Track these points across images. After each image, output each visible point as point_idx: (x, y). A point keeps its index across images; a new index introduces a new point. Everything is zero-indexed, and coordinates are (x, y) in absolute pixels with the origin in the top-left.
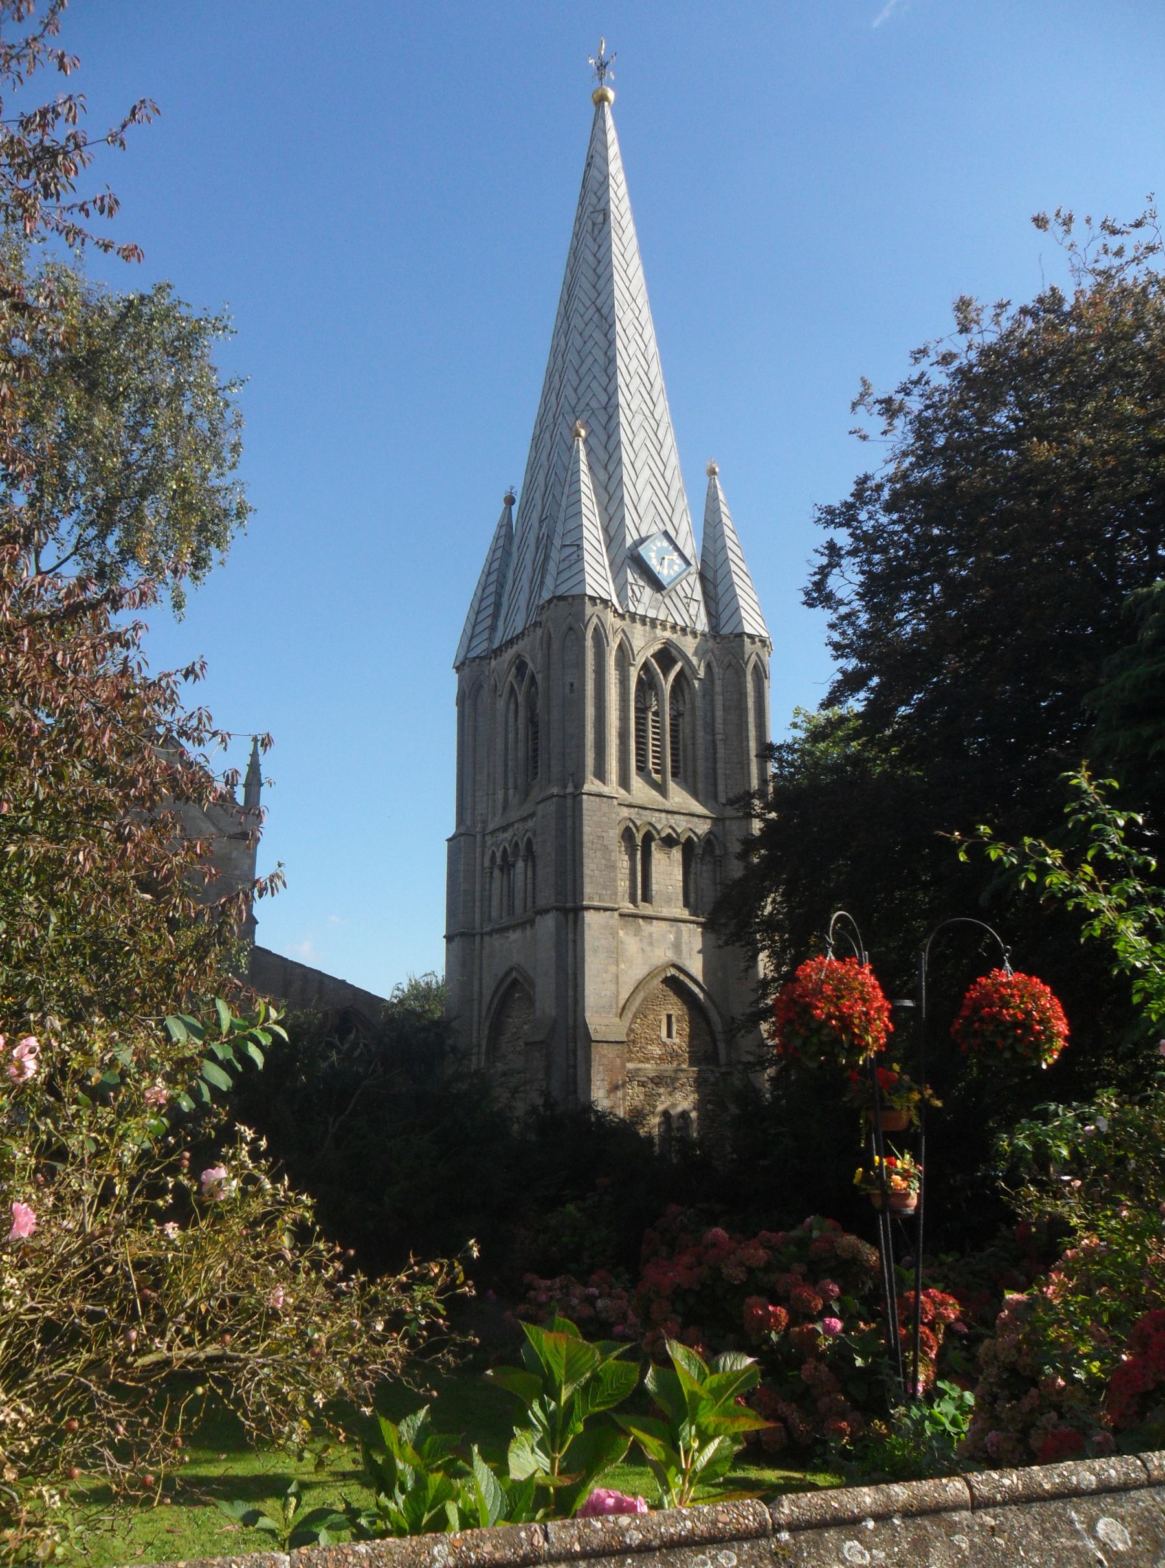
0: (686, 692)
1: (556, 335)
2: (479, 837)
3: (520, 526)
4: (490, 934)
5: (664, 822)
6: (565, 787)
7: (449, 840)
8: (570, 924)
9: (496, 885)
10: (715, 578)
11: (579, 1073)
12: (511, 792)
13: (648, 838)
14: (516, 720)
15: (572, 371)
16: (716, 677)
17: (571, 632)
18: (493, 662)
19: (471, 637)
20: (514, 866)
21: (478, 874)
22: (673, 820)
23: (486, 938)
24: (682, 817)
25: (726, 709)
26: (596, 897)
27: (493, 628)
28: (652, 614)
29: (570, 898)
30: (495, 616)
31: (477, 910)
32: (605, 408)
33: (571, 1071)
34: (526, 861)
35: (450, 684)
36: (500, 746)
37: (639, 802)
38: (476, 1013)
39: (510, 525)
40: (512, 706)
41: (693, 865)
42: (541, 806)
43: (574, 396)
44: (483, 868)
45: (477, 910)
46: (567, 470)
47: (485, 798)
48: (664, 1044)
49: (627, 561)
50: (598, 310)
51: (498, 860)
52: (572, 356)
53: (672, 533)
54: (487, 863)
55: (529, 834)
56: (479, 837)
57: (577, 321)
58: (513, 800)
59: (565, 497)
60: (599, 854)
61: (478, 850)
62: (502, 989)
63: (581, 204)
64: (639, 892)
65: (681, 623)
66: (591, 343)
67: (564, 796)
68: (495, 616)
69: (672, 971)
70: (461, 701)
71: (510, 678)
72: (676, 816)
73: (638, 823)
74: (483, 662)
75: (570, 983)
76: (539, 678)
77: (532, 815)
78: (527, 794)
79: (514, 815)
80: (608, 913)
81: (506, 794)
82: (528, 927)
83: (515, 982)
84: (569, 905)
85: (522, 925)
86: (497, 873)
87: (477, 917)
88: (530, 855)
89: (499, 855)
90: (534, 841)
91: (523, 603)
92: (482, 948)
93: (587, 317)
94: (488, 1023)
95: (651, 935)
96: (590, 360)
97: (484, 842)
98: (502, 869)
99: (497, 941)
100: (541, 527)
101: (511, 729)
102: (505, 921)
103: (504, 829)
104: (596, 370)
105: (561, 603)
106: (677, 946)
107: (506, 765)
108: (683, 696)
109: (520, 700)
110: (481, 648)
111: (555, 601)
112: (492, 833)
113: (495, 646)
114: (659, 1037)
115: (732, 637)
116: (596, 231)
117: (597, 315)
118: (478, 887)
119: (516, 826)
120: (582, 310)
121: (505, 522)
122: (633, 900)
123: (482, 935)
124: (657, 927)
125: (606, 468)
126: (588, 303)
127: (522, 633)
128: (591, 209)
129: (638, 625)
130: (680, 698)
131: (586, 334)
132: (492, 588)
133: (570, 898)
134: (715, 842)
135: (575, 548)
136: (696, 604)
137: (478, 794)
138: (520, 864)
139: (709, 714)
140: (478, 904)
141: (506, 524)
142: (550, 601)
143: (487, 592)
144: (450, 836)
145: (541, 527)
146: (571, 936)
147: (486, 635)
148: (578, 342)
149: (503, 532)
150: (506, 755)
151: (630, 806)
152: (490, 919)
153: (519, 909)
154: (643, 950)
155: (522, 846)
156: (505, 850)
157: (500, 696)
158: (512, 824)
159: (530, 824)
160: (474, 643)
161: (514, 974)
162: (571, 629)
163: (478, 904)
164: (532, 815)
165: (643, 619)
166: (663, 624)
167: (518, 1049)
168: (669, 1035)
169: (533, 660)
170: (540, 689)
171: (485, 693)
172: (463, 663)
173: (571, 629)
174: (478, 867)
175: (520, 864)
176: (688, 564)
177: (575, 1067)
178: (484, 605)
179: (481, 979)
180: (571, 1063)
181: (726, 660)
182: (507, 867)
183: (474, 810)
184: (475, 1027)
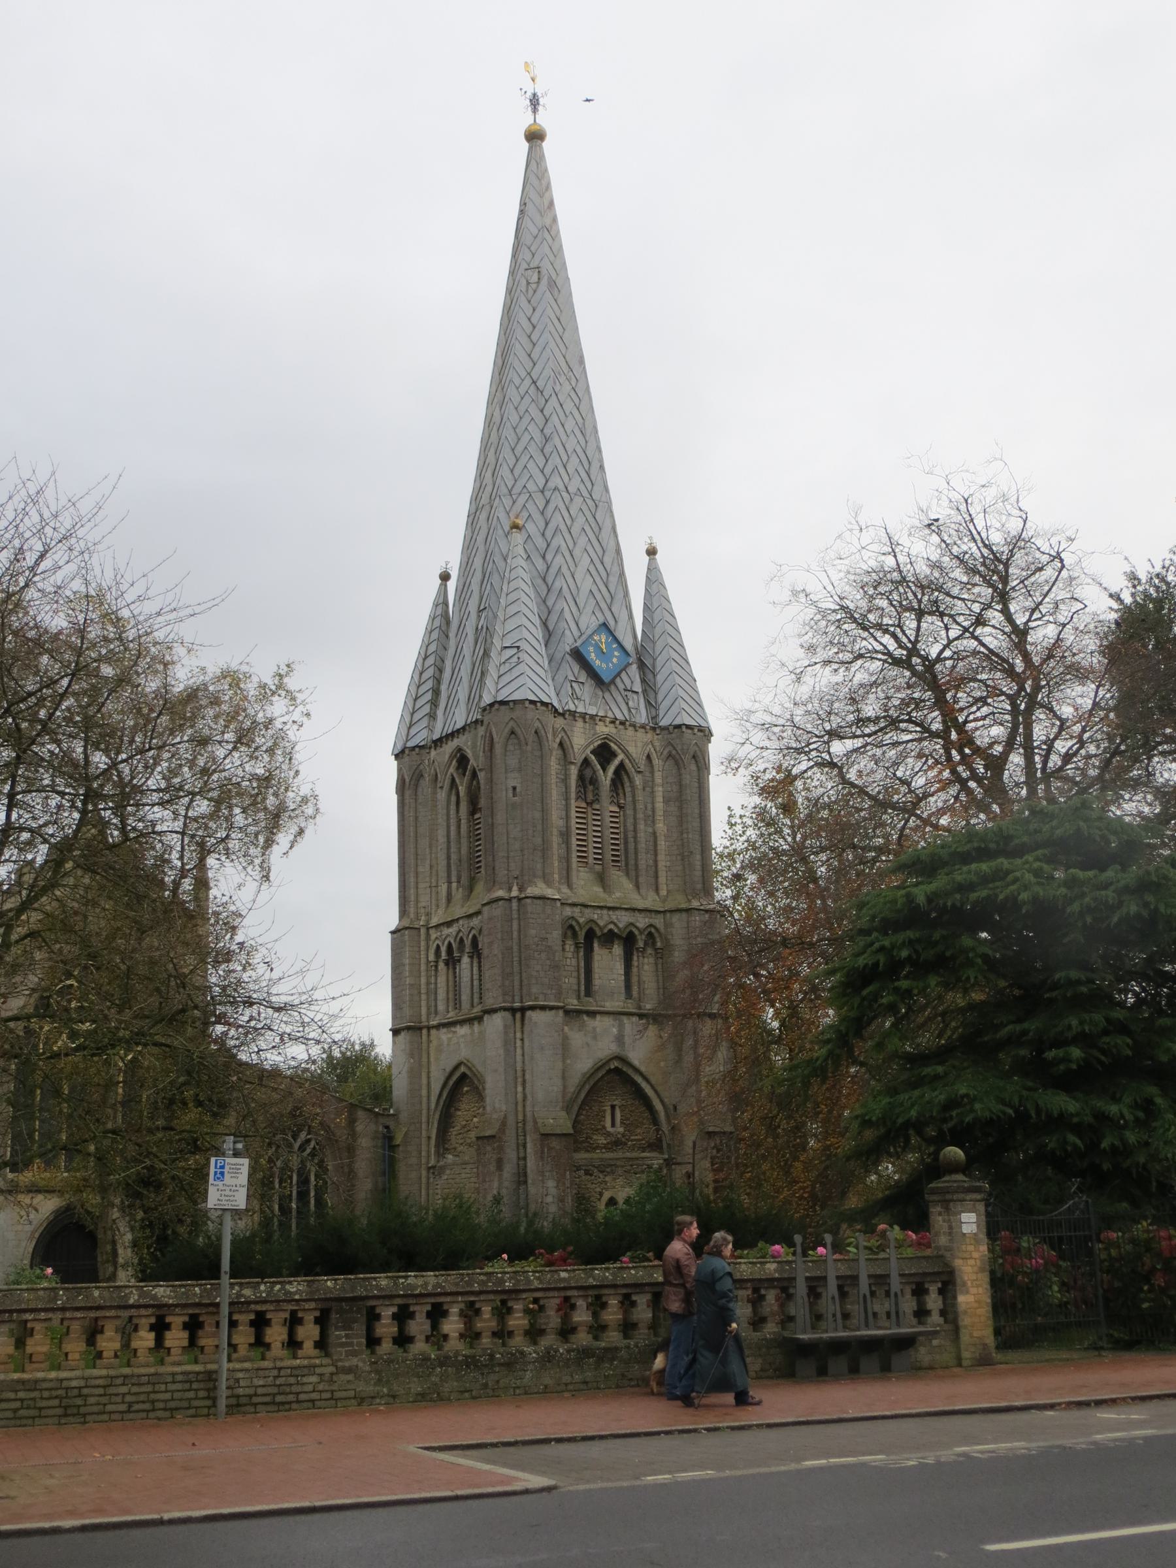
0: (627, 784)
1: (490, 402)
2: (423, 931)
3: (457, 609)
4: (438, 1027)
5: (606, 918)
6: (510, 890)
7: (393, 933)
8: (518, 1024)
9: (442, 979)
10: (654, 667)
11: (529, 1165)
12: (454, 885)
13: (590, 935)
14: (458, 811)
15: (509, 450)
16: (656, 768)
17: (513, 741)
18: (433, 753)
19: (409, 723)
20: (459, 961)
21: (423, 967)
22: (614, 916)
23: (433, 1032)
24: (623, 913)
25: (666, 801)
26: (541, 997)
27: (432, 716)
28: (592, 711)
29: (517, 998)
30: (434, 703)
31: (423, 1003)
32: (542, 492)
33: (522, 1163)
34: (471, 957)
35: (389, 771)
36: (442, 839)
37: (581, 900)
38: (424, 1106)
39: (446, 604)
40: (453, 798)
41: (635, 958)
42: (486, 909)
43: (510, 476)
44: (428, 962)
45: (423, 1003)
46: (502, 579)
47: (428, 890)
48: (609, 1134)
49: (568, 657)
50: (534, 382)
51: (444, 955)
52: (508, 432)
53: (611, 623)
54: (432, 957)
55: (473, 932)
56: (423, 931)
57: (512, 393)
58: (458, 895)
59: (503, 595)
60: (543, 955)
61: (423, 943)
62: (451, 1083)
63: (514, 256)
64: (583, 988)
65: (620, 716)
66: (527, 419)
67: (510, 900)
68: (434, 703)
69: (615, 1064)
70: (402, 787)
71: (452, 770)
72: (618, 913)
73: (581, 920)
74: (424, 751)
75: (520, 1080)
76: (481, 776)
77: (478, 913)
78: (471, 889)
79: (458, 911)
80: (553, 1012)
81: (449, 888)
82: (476, 1023)
83: (464, 1076)
84: (517, 1005)
85: (469, 1021)
86: (441, 965)
87: (424, 1011)
88: (476, 952)
89: (443, 949)
90: (480, 939)
91: (462, 694)
92: (429, 1041)
93: (522, 390)
94: (437, 1116)
95: (594, 1029)
96: (526, 437)
97: (428, 935)
98: (447, 963)
99: (444, 1035)
100: (479, 617)
101: (453, 821)
102: (452, 1015)
103: (449, 924)
104: (533, 449)
105: (503, 707)
106: (620, 1039)
107: (449, 858)
108: (623, 785)
109: (462, 794)
110: (420, 737)
111: (496, 706)
112: (437, 927)
113: (436, 736)
114: (604, 1127)
115: (671, 728)
116: (531, 292)
117: (532, 389)
118: (423, 980)
119: (461, 922)
120: (517, 381)
121: (441, 601)
122: (579, 997)
123: (429, 1028)
124: (599, 1023)
125: (544, 558)
126: (523, 374)
127: (464, 728)
128: (525, 266)
129: (580, 723)
130: (621, 791)
131: (522, 409)
132: (429, 673)
133: (517, 998)
134: (656, 935)
135: (515, 650)
136: (635, 696)
137: (421, 885)
138: (466, 960)
139: (649, 806)
140: (424, 997)
141: (441, 601)
142: (491, 705)
143: (425, 676)
144: (393, 928)
145: (479, 617)
146: (519, 1035)
147: (424, 723)
148: (514, 418)
149: (439, 611)
150: (449, 848)
151: (574, 905)
152: (436, 1013)
153: (466, 1005)
154: (588, 1044)
155: (468, 942)
156: (450, 944)
157: (442, 788)
158: (458, 920)
159: (475, 922)
160: (413, 731)
161: (463, 1069)
162: (513, 733)
163: (424, 997)
164: (478, 913)
165: (583, 716)
166: (603, 719)
167: (469, 1141)
168: (613, 1125)
169: (476, 758)
170: (482, 782)
171: (426, 782)
172: (403, 752)
173: (513, 733)
174: (423, 961)
175: (466, 960)
176: (628, 654)
177: (525, 1158)
178: (421, 691)
179: (429, 1072)
180: (522, 1155)
181: (665, 752)
182: (452, 962)
183: (417, 901)
184: (424, 1126)
